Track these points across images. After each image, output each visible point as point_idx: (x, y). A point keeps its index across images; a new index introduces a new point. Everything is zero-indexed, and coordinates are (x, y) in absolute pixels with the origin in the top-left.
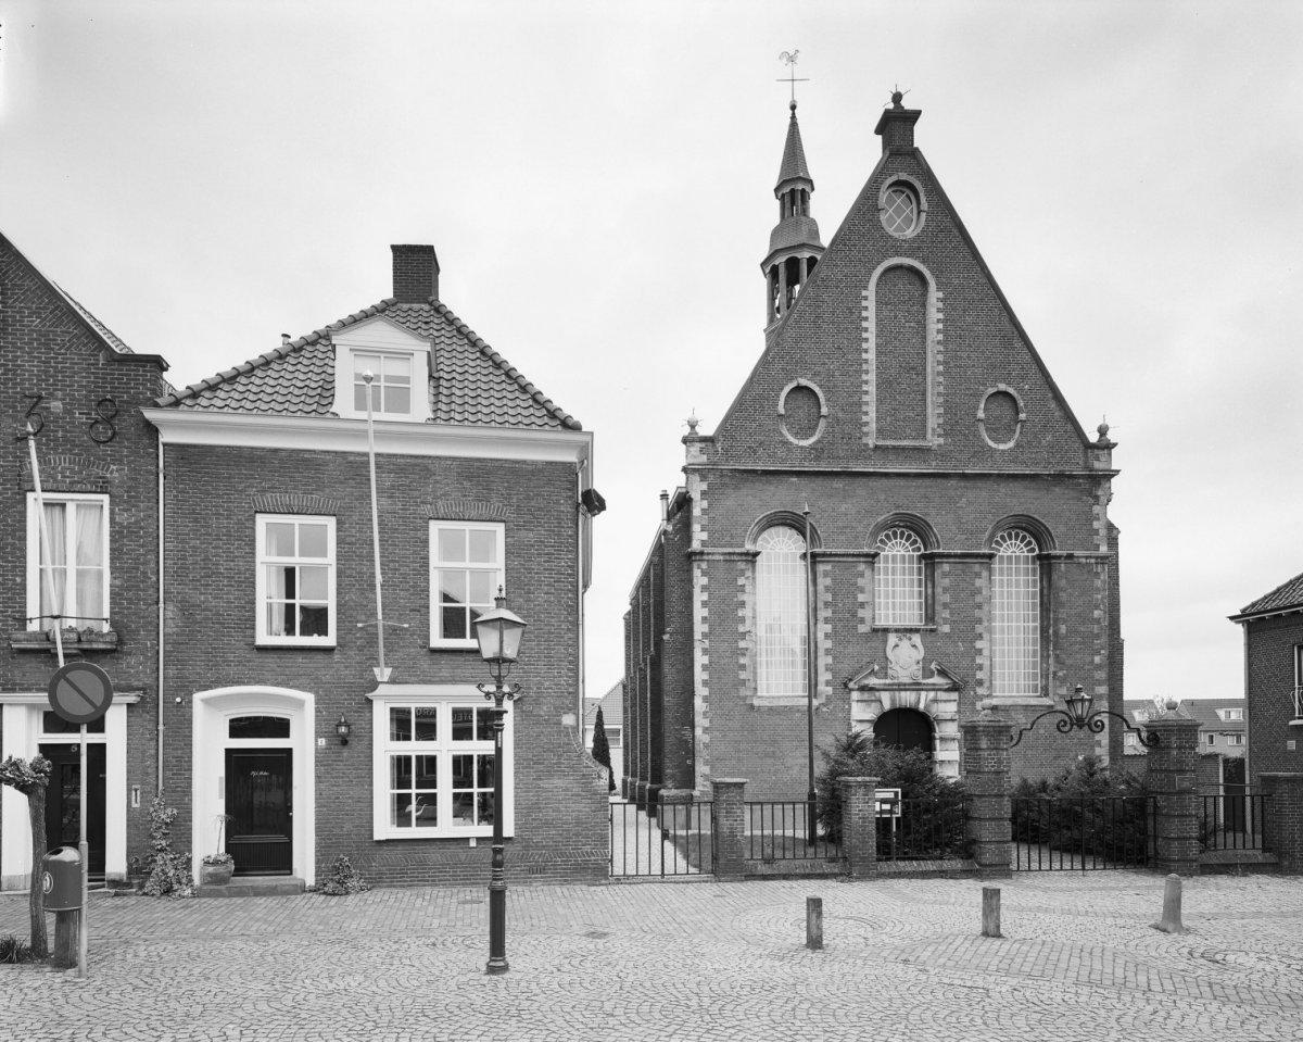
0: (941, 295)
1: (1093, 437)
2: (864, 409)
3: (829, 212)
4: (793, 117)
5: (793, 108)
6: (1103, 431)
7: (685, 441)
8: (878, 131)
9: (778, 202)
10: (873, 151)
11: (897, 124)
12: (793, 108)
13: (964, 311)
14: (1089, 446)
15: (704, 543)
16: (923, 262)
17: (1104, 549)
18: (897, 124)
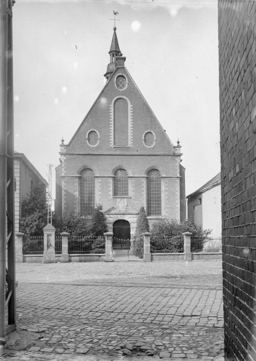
0: (132, 106)
4: (115, 34)
5: (115, 29)
7: (60, 146)
12: (115, 29)
15: (65, 174)
16: (127, 97)
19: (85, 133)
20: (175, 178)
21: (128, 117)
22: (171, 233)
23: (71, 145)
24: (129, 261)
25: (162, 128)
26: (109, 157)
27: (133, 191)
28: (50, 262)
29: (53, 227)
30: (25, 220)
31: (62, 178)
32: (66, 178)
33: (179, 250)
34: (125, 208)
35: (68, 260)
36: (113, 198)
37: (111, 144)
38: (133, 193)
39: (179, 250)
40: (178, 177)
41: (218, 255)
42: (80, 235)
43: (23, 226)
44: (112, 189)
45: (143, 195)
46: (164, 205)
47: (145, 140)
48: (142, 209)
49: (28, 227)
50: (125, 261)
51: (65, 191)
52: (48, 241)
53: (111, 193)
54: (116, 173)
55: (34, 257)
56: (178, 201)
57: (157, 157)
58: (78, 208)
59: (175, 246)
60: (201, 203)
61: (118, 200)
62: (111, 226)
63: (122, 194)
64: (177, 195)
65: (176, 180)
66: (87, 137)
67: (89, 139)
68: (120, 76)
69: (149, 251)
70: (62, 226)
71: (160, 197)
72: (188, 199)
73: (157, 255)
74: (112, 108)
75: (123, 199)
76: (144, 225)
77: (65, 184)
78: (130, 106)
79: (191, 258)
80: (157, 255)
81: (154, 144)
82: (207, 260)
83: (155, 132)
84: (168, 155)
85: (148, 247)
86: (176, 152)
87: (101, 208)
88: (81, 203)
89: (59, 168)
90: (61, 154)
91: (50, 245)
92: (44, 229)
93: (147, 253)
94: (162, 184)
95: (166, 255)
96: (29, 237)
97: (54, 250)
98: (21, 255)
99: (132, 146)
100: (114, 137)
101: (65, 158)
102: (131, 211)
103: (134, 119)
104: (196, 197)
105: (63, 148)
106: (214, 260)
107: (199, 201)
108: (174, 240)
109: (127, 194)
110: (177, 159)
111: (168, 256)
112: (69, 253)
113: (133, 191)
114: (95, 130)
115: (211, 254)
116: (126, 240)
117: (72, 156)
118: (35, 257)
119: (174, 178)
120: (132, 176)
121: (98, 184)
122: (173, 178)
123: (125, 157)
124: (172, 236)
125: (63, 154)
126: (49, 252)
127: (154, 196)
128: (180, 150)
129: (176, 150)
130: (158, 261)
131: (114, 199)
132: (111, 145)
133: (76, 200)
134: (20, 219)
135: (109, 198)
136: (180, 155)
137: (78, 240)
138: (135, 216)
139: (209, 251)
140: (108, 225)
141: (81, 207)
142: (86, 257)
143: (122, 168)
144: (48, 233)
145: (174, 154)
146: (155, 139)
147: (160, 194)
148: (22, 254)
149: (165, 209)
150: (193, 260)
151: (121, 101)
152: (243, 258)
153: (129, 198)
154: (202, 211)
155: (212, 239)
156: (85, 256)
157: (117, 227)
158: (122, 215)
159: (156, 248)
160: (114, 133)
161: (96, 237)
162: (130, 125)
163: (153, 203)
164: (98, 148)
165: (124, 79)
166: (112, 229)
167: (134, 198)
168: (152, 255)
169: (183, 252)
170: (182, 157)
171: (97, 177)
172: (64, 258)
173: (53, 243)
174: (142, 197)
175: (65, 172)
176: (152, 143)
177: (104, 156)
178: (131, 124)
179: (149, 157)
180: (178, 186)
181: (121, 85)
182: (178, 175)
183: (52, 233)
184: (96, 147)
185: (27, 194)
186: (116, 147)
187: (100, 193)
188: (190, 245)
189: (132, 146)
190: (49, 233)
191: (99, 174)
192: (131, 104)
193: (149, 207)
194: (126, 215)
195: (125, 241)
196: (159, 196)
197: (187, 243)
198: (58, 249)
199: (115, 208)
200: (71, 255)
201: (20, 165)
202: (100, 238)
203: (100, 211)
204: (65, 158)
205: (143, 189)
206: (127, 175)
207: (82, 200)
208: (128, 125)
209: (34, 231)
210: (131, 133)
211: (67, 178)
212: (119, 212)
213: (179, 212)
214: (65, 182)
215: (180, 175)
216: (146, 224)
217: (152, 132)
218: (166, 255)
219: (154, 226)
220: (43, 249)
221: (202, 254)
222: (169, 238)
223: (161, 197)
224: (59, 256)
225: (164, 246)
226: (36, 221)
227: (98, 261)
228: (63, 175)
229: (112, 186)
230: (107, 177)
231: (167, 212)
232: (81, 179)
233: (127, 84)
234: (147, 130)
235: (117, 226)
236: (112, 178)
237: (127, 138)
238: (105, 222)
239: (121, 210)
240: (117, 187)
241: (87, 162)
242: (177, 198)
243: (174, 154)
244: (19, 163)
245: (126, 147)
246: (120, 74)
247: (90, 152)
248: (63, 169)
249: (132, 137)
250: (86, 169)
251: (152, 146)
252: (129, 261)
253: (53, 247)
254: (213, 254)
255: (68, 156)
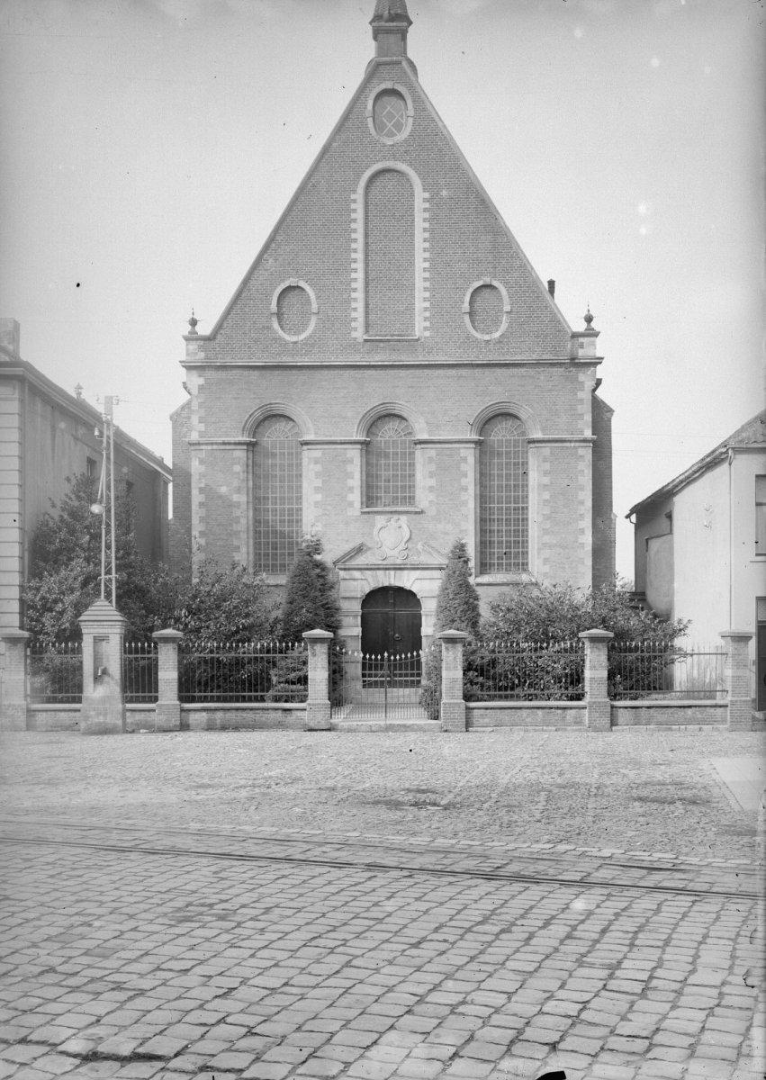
0: (427, 195)
7: (187, 339)
13: (451, 209)
15: (201, 434)
16: (411, 165)
19: (268, 296)
20: (576, 441)
21: (413, 235)
22: (545, 633)
23: (219, 336)
24: (389, 728)
25: (532, 269)
26: (348, 373)
27: (431, 489)
28: (105, 731)
29: (112, 613)
30: (38, 589)
31: (192, 448)
32: (203, 447)
33: (571, 691)
34: (402, 546)
35: (178, 723)
36: (363, 513)
37: (355, 329)
38: (432, 497)
39: (571, 691)
40: (585, 441)
41: (708, 709)
42: (228, 637)
43: (33, 607)
44: (359, 483)
45: (465, 503)
46: (538, 537)
47: (471, 314)
48: (459, 552)
49: (51, 610)
50: (373, 728)
51: (201, 490)
52: (97, 659)
53: (356, 497)
54: (374, 429)
55: (63, 713)
56: (587, 523)
57: (515, 371)
58: (244, 550)
59: (558, 679)
60: (671, 532)
61: (380, 520)
62: (356, 607)
63: (395, 501)
65: (581, 452)
66: (274, 307)
67: (279, 315)
68: (385, 92)
69: (460, 694)
70: (171, 610)
71: (525, 509)
72: (637, 518)
73: (487, 709)
74: (359, 207)
75: (396, 517)
76: (463, 603)
77: (203, 468)
78: (420, 196)
79: (607, 721)
80: (487, 709)
81: (504, 326)
82: (667, 726)
83: (506, 283)
84: (552, 365)
85: (454, 681)
86: (581, 353)
87: (316, 548)
88: (256, 532)
89: (185, 414)
90: (189, 368)
91: (105, 672)
93: (452, 701)
94: (530, 463)
95: (521, 708)
96: (54, 646)
97: (118, 689)
98: (19, 706)
99: (427, 334)
100: (367, 305)
101: (201, 381)
102: (425, 559)
103: (434, 237)
104: (654, 512)
105: (193, 346)
106: (691, 727)
107: (665, 521)
108: (552, 658)
110: (586, 379)
111: (525, 713)
112: (182, 699)
113: (431, 489)
114: (302, 284)
115: (680, 707)
116: (379, 657)
117: (222, 374)
118: (67, 713)
119: (572, 445)
120: (425, 437)
121: (312, 466)
122: (568, 444)
123: (403, 373)
124: (548, 645)
126: (103, 695)
127: (513, 505)
128: (593, 344)
129: (582, 346)
130: (490, 729)
131: (366, 516)
132: (354, 334)
133: (238, 522)
134: (21, 587)
135: (349, 514)
136: (597, 362)
137: (223, 657)
138: (437, 574)
139: (689, 693)
140: (345, 605)
141: (257, 545)
142: (244, 714)
143: (394, 412)
144: (96, 631)
145: (574, 359)
146: (507, 308)
148: (178, 702)
149: (539, 549)
150: (614, 728)
151: (388, 183)
153: (416, 513)
154: (672, 554)
155: (692, 655)
156: (237, 709)
157: (375, 612)
158: (392, 572)
159: (491, 683)
160: (367, 292)
161: (287, 646)
163: (498, 531)
164: (309, 344)
165: (402, 103)
166: (359, 618)
167: (432, 512)
168: (468, 708)
169: (579, 697)
170: (600, 371)
171: (307, 443)
172: (165, 717)
173: (114, 664)
174: (459, 510)
175: (202, 427)
176: (497, 323)
179: (487, 371)
180: (586, 471)
181: (389, 125)
182: (588, 434)
184: (305, 342)
185: (50, 499)
186: (373, 341)
187: (319, 497)
188: (605, 674)
189: (427, 334)
190: (101, 631)
191: (316, 433)
192: (425, 190)
193: (483, 545)
194: (406, 572)
195: (376, 659)
196: (521, 505)
197: (595, 667)
198: (139, 682)
199: (369, 549)
200: (129, 706)
201: (22, 401)
202: (301, 649)
203: (318, 557)
204: (201, 381)
205: (464, 481)
206: (410, 433)
207: (260, 522)
208: (412, 264)
209: (67, 624)
210: (426, 289)
211: (209, 447)
212: (380, 562)
213: (589, 562)
214: (202, 462)
215: (593, 434)
216: (466, 603)
217: (495, 283)
218: (521, 708)
219: (495, 608)
220: (80, 688)
221: (648, 707)
222: (536, 650)
223: (527, 508)
224: (149, 711)
225: (519, 678)
226: (72, 590)
227: (280, 726)
228: (194, 437)
229: (357, 475)
230: (342, 443)
231: (546, 561)
232: (255, 449)
233: (411, 120)
234: (478, 278)
235: (378, 609)
236: (359, 446)
238: (333, 593)
239: (390, 553)
240: (377, 477)
241: (271, 392)
242: (582, 513)
243: (574, 359)
244: (17, 395)
245: (406, 341)
246: (388, 85)
247: (284, 359)
248: (195, 419)
249: (427, 304)
250: (272, 416)
251: (497, 335)
252: (389, 728)
253: (113, 679)
254: (690, 707)
255: (210, 374)
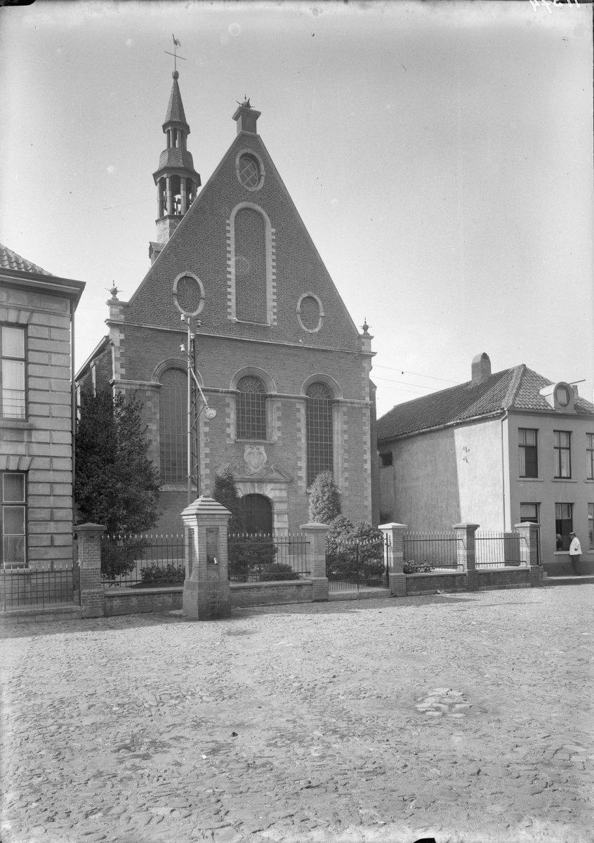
0: (274, 230)
1: (361, 332)
2: (229, 297)
3: (206, 165)
4: (176, 87)
5: (176, 76)
6: (366, 328)
8: (236, 118)
9: (165, 136)
10: (231, 131)
11: (247, 116)
12: (176, 76)
14: (360, 337)
17: (367, 399)
18: (247, 116)
19: (171, 281)
45: (299, 439)
64: (365, 443)
78: (270, 231)
92: (182, 513)
99: (275, 324)
101: (122, 336)
105: (116, 310)
109: (263, 435)
125: (118, 326)
132: (229, 317)
147: (331, 439)
152: (422, 565)
162: (270, 276)
177: (40, 392)
178: (274, 274)
183: (220, 523)
190: (212, 523)
204: (122, 336)
237: (264, 304)
251: (317, 330)
